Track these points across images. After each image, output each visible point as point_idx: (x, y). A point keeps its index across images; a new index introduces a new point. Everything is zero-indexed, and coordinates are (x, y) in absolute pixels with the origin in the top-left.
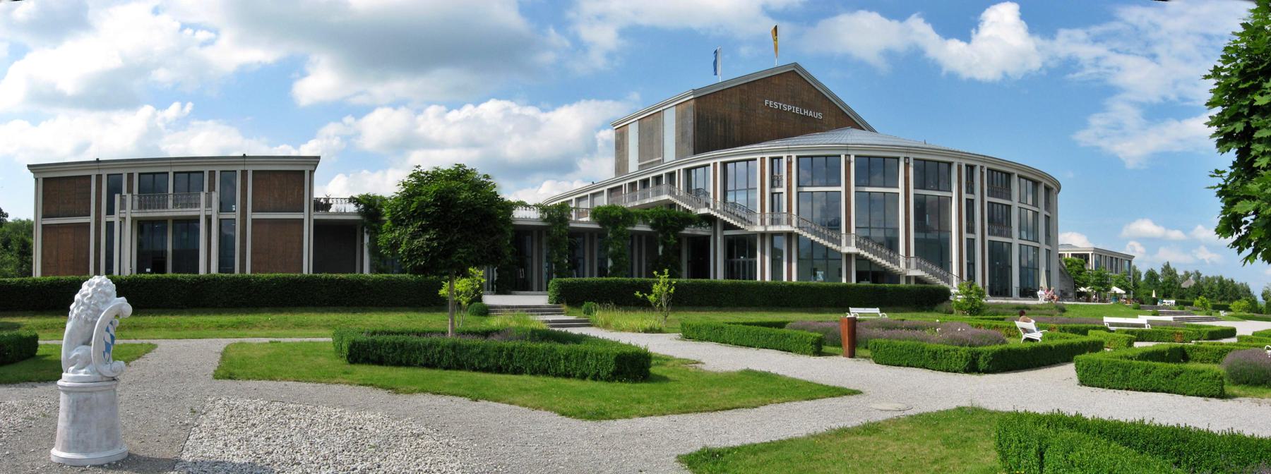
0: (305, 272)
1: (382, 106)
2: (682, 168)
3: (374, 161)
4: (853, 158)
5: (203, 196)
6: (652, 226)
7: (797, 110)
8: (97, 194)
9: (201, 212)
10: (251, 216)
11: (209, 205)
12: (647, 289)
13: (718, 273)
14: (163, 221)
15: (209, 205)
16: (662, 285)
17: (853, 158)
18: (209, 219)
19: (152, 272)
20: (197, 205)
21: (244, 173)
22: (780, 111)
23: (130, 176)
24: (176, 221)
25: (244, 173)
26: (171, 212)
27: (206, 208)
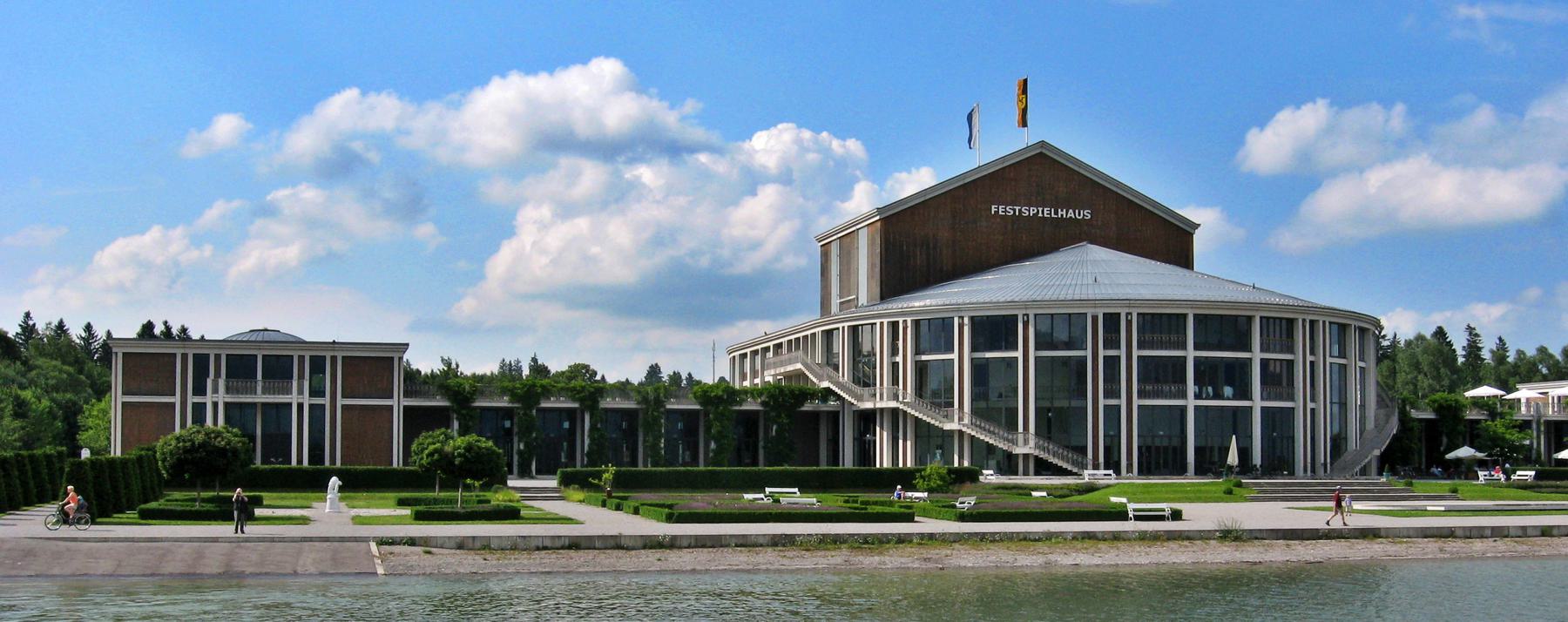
0: (395, 465)
1: (213, 576)
2: (846, 325)
3: (473, 329)
4: (966, 320)
5: (295, 384)
6: (763, 404)
7: (1046, 212)
8: (183, 376)
9: (293, 398)
10: (340, 402)
11: (300, 392)
12: (598, 475)
13: (848, 461)
14: (254, 405)
15: (300, 392)
16: (609, 472)
17: (966, 320)
18: (300, 406)
19: (1235, 398)
20: (289, 392)
21: (334, 359)
22: (1017, 219)
23: (218, 357)
24: (264, 405)
25: (334, 359)
26: (260, 398)
27: (297, 396)
